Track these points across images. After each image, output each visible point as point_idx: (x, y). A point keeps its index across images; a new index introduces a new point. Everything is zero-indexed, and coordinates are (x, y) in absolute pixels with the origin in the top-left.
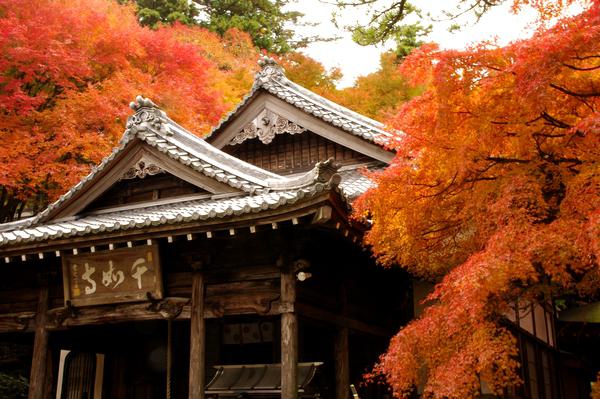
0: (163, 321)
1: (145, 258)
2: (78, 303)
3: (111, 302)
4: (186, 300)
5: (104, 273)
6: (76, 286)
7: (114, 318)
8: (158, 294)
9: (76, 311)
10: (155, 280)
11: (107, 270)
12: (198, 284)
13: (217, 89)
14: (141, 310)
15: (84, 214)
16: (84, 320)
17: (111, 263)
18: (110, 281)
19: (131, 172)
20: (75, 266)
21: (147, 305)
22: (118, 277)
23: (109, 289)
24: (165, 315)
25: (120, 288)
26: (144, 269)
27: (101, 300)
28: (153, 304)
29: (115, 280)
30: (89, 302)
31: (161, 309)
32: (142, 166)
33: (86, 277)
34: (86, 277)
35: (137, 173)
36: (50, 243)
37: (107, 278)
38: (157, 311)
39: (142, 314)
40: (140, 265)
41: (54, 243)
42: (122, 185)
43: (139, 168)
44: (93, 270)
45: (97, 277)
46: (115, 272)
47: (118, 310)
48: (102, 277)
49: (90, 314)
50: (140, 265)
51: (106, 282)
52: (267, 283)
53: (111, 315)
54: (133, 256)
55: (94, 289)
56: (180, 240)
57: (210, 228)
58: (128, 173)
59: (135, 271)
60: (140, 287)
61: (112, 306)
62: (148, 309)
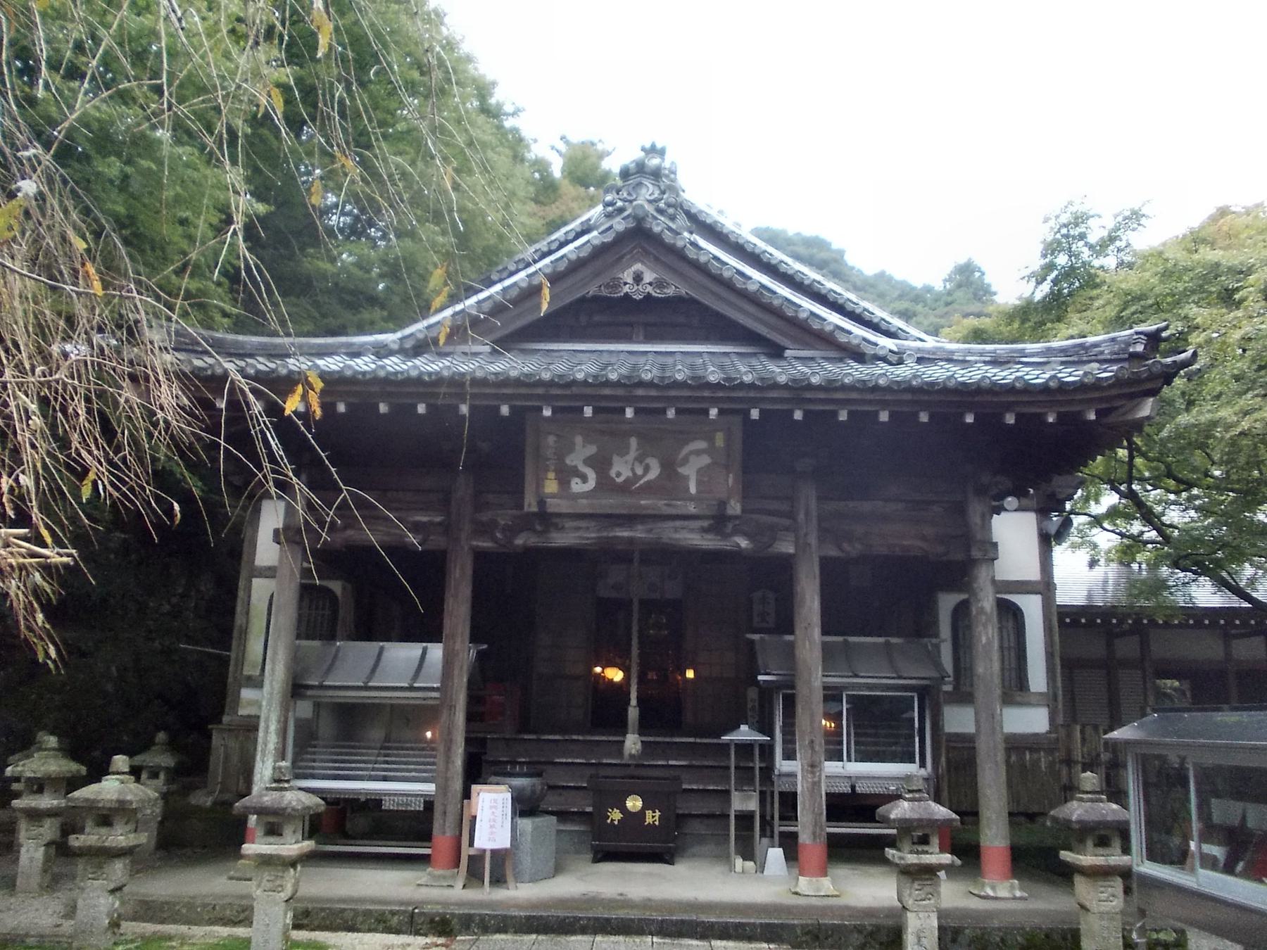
0: (735, 556)
1: (711, 440)
2: (555, 506)
3: (633, 512)
4: (787, 522)
5: (616, 459)
6: (551, 475)
7: (631, 541)
8: (735, 508)
9: (546, 519)
10: (731, 481)
11: (623, 452)
12: (808, 498)
13: (667, 164)
14: (692, 531)
15: (506, 343)
16: (562, 539)
17: (633, 442)
18: (626, 473)
19: (616, 284)
20: (551, 440)
21: (706, 524)
22: (647, 469)
23: (624, 489)
24: (744, 543)
25: (649, 488)
26: (705, 460)
27: (610, 503)
28: (719, 522)
29: (639, 471)
30: (583, 506)
31: (736, 531)
32: (638, 278)
33: (575, 460)
34: (575, 460)
35: (626, 289)
36: (575, 390)
37: (621, 469)
38: (725, 536)
39: (694, 538)
40: (698, 453)
41: (588, 391)
42: (599, 303)
43: (630, 280)
44: (592, 450)
45: (601, 463)
46: (640, 459)
47: (640, 527)
48: (610, 464)
49: (578, 529)
50: (698, 453)
51: (619, 474)
52: (936, 508)
53: (626, 534)
54: (685, 437)
55: (591, 484)
56: (862, 419)
57: (925, 406)
58: (607, 286)
59: (685, 461)
60: (693, 490)
61: (630, 519)
62: (705, 530)
